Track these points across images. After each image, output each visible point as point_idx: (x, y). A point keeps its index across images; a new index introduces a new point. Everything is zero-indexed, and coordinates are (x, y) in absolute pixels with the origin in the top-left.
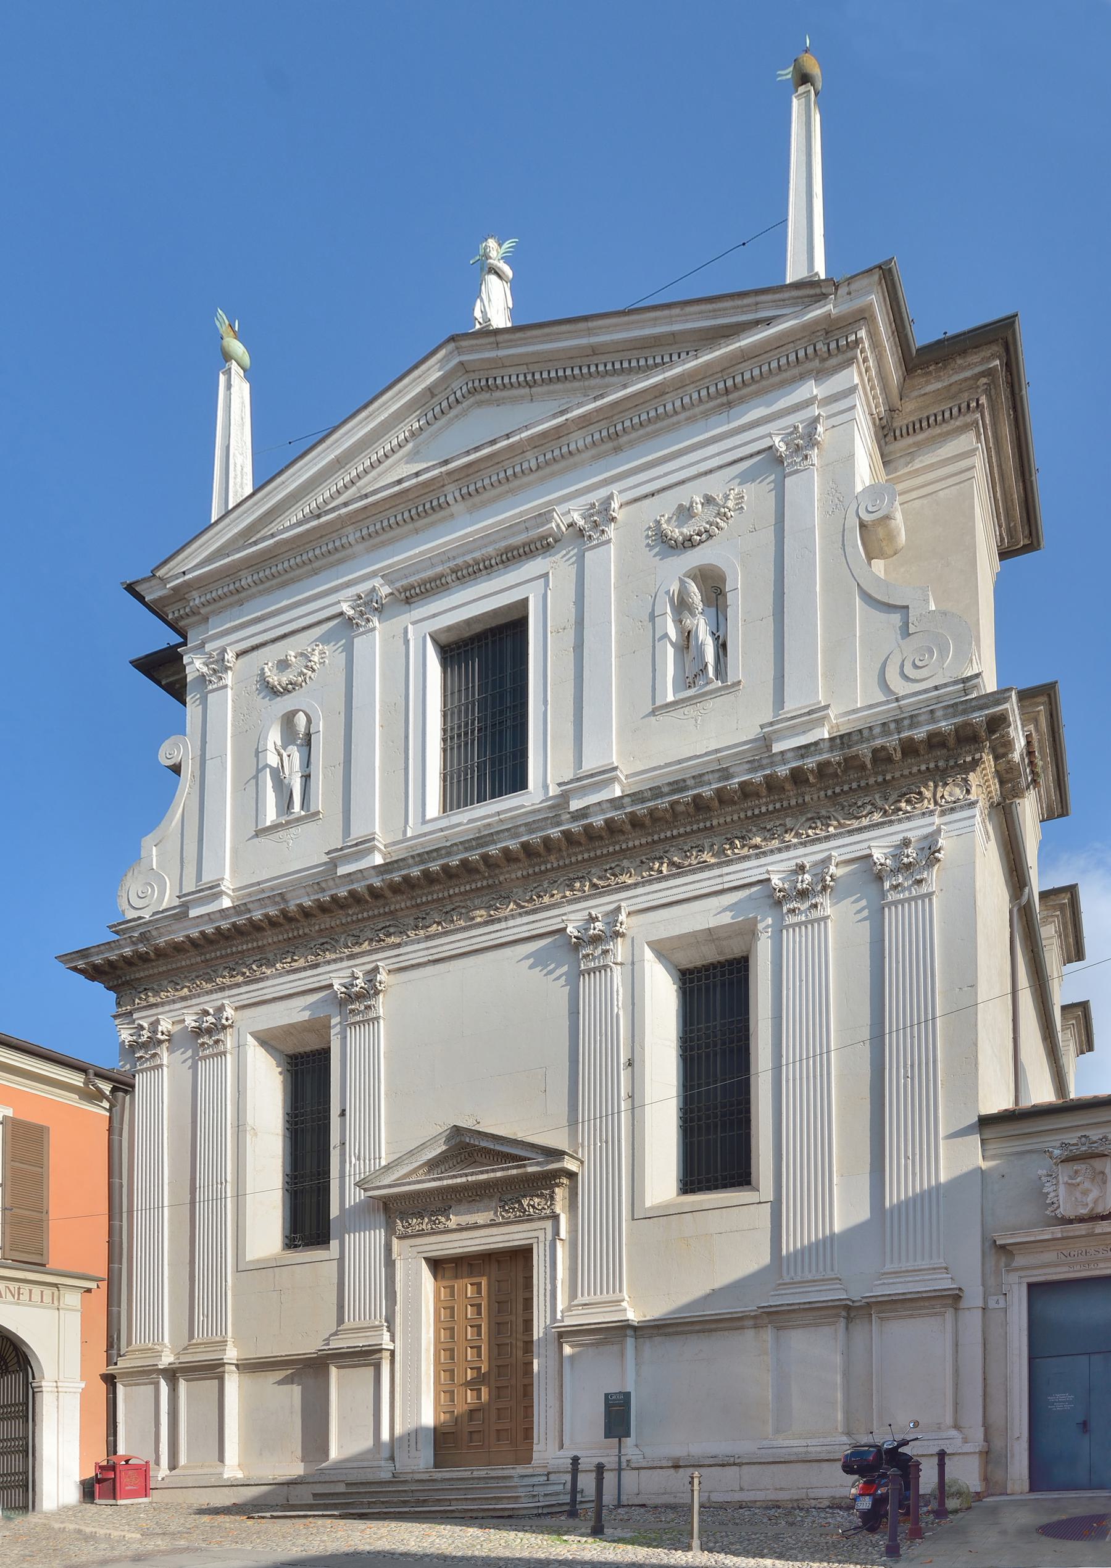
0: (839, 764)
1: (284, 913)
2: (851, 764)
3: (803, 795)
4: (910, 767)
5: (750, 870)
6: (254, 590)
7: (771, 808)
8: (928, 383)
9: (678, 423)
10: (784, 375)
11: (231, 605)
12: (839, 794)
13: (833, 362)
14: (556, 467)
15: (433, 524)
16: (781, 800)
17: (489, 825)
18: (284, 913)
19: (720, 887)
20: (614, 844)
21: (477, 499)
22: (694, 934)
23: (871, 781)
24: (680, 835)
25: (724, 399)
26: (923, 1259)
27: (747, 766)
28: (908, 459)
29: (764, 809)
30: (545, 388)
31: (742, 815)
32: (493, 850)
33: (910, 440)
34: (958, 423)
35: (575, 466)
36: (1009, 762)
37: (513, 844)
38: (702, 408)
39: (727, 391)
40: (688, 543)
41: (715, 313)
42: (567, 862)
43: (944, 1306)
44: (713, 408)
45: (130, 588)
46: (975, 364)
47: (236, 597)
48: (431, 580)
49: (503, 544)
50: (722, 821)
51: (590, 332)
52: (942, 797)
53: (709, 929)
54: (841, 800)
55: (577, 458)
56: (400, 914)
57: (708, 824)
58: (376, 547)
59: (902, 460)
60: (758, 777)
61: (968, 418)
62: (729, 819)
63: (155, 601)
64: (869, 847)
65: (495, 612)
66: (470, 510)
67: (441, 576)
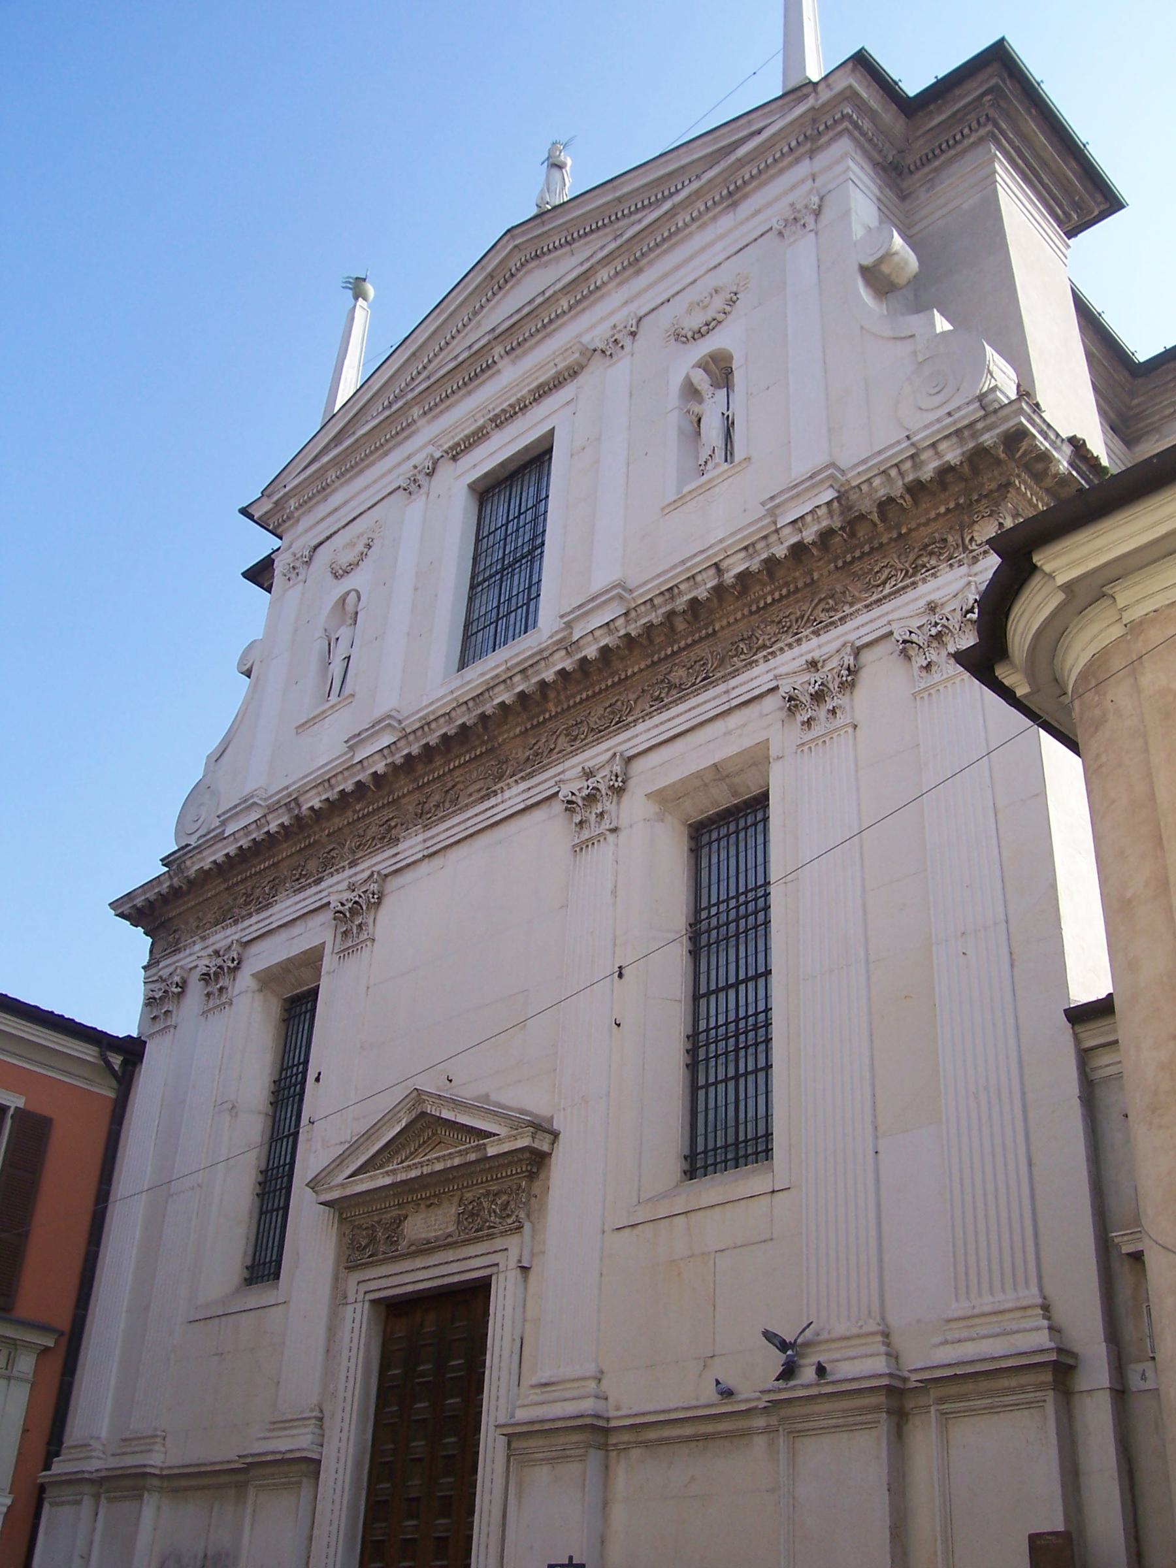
0: (842, 528)
1: (298, 818)
2: (854, 522)
3: (810, 572)
4: (927, 511)
5: (758, 677)
6: (337, 483)
7: (777, 596)
8: (932, 119)
9: (690, 233)
10: (781, 165)
11: (318, 503)
12: (852, 562)
13: (824, 139)
14: (586, 303)
15: (483, 382)
16: (787, 584)
17: (497, 676)
18: (298, 818)
19: (726, 707)
20: (612, 675)
21: (519, 351)
22: (698, 775)
23: (885, 540)
24: (681, 650)
25: (730, 201)
26: (1003, 1290)
27: (742, 554)
28: (928, 185)
29: (769, 600)
30: (583, 241)
31: (746, 612)
32: (488, 708)
33: (926, 170)
34: (972, 140)
35: (603, 296)
36: (1055, 475)
37: (506, 697)
38: (711, 214)
39: (730, 194)
40: (699, 334)
41: (716, 140)
42: (565, 707)
43: (1039, 1387)
44: (721, 212)
45: (244, 512)
46: (976, 89)
47: (322, 495)
48: (473, 434)
49: (535, 384)
50: (724, 623)
51: (615, 189)
52: (972, 539)
53: (715, 765)
54: (856, 567)
55: (604, 290)
56: (403, 801)
57: (710, 630)
58: (436, 417)
59: (923, 189)
60: (755, 565)
61: (982, 132)
62: (732, 620)
63: (260, 518)
64: (889, 623)
65: (527, 449)
66: (513, 362)
67: (483, 427)
